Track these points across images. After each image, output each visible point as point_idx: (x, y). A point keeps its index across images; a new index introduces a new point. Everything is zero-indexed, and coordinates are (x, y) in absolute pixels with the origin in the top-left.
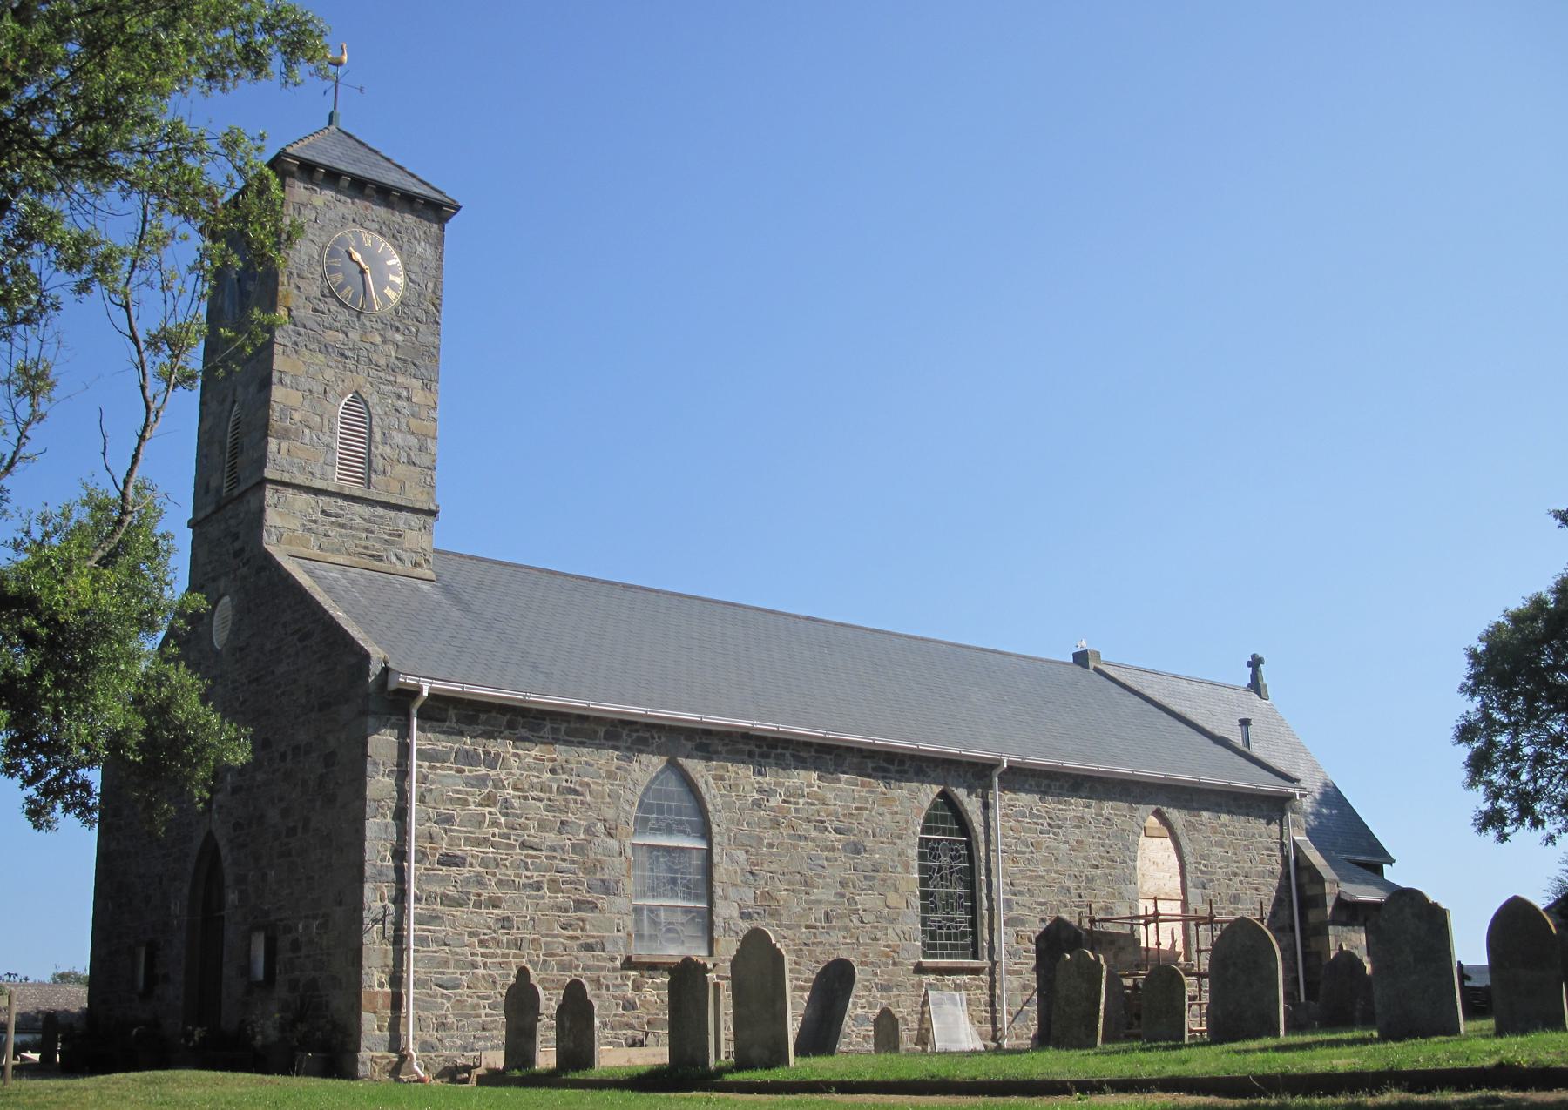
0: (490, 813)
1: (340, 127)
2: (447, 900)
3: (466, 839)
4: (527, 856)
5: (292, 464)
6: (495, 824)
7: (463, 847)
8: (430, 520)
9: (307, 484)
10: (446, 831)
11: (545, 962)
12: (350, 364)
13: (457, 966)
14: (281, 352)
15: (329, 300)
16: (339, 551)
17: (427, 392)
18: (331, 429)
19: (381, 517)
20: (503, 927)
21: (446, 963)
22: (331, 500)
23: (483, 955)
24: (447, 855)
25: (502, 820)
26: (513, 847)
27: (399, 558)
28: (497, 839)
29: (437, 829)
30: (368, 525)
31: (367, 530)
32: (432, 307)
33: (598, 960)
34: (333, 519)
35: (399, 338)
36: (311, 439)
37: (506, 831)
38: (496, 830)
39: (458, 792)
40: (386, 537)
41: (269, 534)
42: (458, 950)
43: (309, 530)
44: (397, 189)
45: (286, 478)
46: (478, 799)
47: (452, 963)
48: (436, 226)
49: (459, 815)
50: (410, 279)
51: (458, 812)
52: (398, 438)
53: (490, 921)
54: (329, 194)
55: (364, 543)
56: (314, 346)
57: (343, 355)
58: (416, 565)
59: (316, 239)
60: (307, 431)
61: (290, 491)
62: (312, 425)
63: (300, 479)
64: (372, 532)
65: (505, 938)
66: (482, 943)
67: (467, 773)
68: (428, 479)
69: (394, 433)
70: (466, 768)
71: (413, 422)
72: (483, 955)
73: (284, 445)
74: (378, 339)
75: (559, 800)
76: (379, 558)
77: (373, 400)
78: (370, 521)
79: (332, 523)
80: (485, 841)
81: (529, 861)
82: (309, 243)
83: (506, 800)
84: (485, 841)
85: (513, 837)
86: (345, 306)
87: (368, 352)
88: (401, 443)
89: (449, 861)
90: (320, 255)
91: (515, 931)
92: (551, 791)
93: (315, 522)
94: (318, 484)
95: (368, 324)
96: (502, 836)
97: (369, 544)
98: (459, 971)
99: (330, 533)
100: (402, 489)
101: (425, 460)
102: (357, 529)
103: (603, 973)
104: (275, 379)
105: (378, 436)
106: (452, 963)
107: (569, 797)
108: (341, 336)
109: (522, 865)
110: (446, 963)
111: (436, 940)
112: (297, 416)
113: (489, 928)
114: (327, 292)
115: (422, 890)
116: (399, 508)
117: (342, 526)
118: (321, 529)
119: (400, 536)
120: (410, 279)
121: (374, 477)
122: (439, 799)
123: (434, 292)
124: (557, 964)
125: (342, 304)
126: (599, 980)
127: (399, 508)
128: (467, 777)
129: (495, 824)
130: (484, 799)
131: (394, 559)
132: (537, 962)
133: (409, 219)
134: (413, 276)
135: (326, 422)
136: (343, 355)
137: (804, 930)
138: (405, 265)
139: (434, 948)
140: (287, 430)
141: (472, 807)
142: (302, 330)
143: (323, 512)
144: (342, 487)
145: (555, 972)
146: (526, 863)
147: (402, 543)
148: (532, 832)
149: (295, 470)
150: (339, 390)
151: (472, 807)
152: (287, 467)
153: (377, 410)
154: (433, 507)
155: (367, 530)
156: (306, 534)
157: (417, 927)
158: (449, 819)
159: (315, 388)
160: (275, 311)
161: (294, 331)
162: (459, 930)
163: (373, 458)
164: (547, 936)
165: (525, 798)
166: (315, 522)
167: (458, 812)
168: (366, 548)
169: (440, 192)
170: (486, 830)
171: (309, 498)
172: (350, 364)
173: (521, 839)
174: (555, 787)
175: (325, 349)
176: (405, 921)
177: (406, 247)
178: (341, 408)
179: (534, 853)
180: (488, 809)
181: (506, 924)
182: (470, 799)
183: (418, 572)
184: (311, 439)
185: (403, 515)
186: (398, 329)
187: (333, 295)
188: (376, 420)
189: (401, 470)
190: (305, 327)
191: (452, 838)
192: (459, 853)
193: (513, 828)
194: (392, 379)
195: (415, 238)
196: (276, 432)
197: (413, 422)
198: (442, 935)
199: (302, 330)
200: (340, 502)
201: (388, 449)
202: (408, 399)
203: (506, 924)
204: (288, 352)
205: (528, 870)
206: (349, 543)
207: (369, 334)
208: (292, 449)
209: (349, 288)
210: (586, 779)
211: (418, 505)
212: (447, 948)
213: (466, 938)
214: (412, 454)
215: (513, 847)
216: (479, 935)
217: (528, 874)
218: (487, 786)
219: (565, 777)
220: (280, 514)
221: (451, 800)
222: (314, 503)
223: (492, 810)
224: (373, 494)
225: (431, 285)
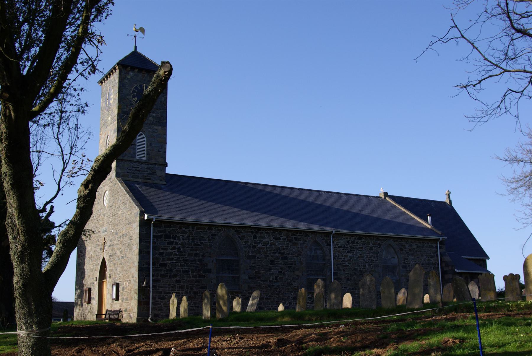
6: (175, 254)
11: (190, 292)
37: (178, 256)
38: (176, 256)
46: (171, 248)
76: (150, 179)
84: (172, 259)
106: (163, 293)
129: (175, 254)
145: (193, 295)
151: (169, 250)
156: (128, 174)
182: (168, 248)
213: (167, 286)
215: (180, 261)
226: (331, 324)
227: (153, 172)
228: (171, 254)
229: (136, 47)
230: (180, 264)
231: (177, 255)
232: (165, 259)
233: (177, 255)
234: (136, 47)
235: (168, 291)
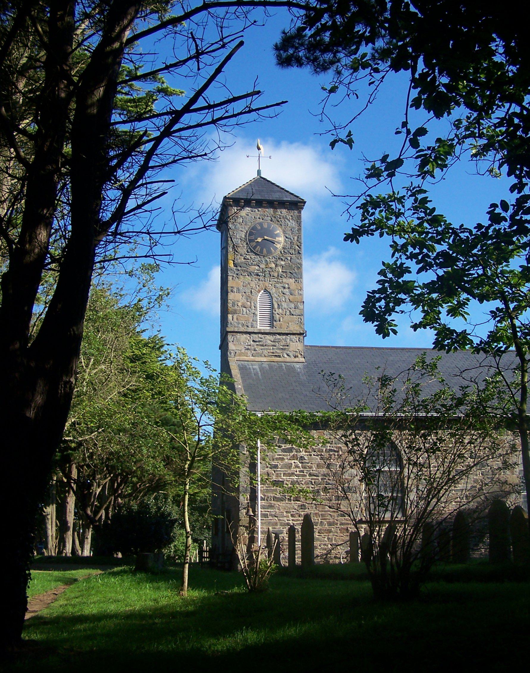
0: (294, 463)
1: (262, 176)
2: (275, 499)
3: (284, 474)
4: (312, 479)
5: (239, 323)
6: (297, 467)
7: (282, 477)
8: (301, 337)
9: (245, 331)
10: (274, 471)
11: (321, 522)
12: (261, 278)
13: (281, 525)
14: (231, 279)
15: (250, 254)
16: (261, 356)
17: (297, 283)
18: (255, 307)
19: (279, 339)
20: (302, 509)
21: (276, 524)
22: (256, 336)
23: (293, 520)
24: (275, 481)
25: (300, 465)
26: (306, 476)
27: (288, 355)
28: (298, 473)
29: (271, 471)
30: (273, 343)
31: (273, 346)
32: (297, 247)
33: (347, 520)
34: (257, 343)
35: (283, 263)
36: (246, 312)
37: (302, 469)
38: (298, 469)
39: (280, 455)
40: (282, 347)
41: (230, 353)
42: (281, 518)
43: (248, 349)
44: (276, 201)
45: (236, 330)
46: (289, 457)
47: (279, 524)
48: (296, 212)
49: (280, 464)
50: (286, 237)
51: (280, 463)
52: (284, 305)
53: (296, 507)
54: (248, 209)
55: (272, 351)
56: (246, 274)
57: (258, 275)
58: (296, 357)
59: (243, 230)
60: (244, 309)
61: (239, 334)
62: (246, 306)
63: (242, 329)
64: (275, 346)
65: (302, 513)
66: (292, 516)
67: (283, 447)
68: (300, 320)
69: (283, 303)
70: (283, 445)
71: (291, 297)
72: (293, 520)
73: (235, 316)
74: (273, 265)
75: (326, 455)
76: (279, 356)
77: (273, 291)
78: (274, 342)
79: (257, 345)
80: (293, 474)
81: (313, 481)
82: (240, 232)
83: (301, 457)
84: (293, 474)
85: (305, 472)
86: (258, 255)
87: (269, 272)
88: (286, 307)
89: (276, 483)
90: (245, 236)
91: (307, 510)
92: (322, 452)
93: (250, 345)
94: (250, 330)
95: (268, 260)
96: (300, 471)
97: (274, 351)
98: (282, 527)
99: (257, 349)
100: (288, 327)
101: (297, 312)
102: (269, 346)
103: (350, 526)
104: (229, 291)
105: (276, 306)
106: (279, 524)
107: (332, 453)
108: (257, 268)
109: (310, 483)
110: (276, 524)
111: (271, 515)
112: (240, 304)
113: (295, 509)
114: (249, 250)
115: (265, 496)
116: (287, 334)
117: (262, 345)
118: (252, 348)
119: (288, 346)
120: (286, 237)
121: (275, 323)
122: (271, 459)
123: (297, 241)
124: (327, 523)
125: (256, 254)
126: (347, 529)
127: (287, 334)
128: (283, 449)
129: (297, 467)
130: (291, 457)
131: (286, 356)
132: (318, 522)
133: (284, 211)
134: (287, 236)
135: (253, 304)
136: (258, 275)
137: (454, 503)
138: (284, 232)
139: (270, 518)
140: (235, 310)
141: (286, 461)
142: (239, 268)
143: (253, 341)
144: (260, 330)
145: (326, 526)
146: (312, 482)
147: (288, 349)
148: (314, 469)
149: (240, 326)
150: (257, 290)
151: (286, 461)
152: (236, 325)
153: (275, 295)
154: (302, 332)
155: (273, 346)
156: (246, 351)
157: (263, 510)
158: (276, 466)
159: (247, 291)
160: (277, 248)
161: (236, 269)
162: (282, 510)
163: (274, 315)
164: (322, 511)
165: (311, 455)
166: (250, 345)
167: (280, 463)
168: (273, 353)
169: (297, 197)
170: (293, 470)
171: (247, 336)
172: (261, 278)
173: (309, 472)
174: (325, 449)
175: (250, 274)
176: (256, 508)
177: (283, 224)
178: (259, 297)
179: (315, 478)
180: (294, 461)
181: (303, 507)
182: (285, 458)
183: (296, 360)
184: (246, 312)
185: (288, 337)
186: (282, 259)
187: (252, 251)
188: (274, 299)
189: (288, 317)
190: (241, 267)
191: (277, 474)
192: (281, 480)
193: (305, 468)
194: (281, 281)
195: (287, 219)
196: (231, 311)
197: (291, 297)
198: (273, 513)
199: (239, 268)
200: (260, 335)
201: (280, 310)
202: (289, 288)
203: (303, 507)
204: (234, 278)
205: (313, 485)
206: (265, 352)
207: (269, 264)
208: (238, 317)
209: (258, 247)
210: (340, 445)
211: (295, 332)
212: (276, 518)
213: (285, 513)
214: (291, 310)
215: (306, 476)
216: (290, 512)
217: (313, 486)
218: (292, 452)
219: (329, 445)
220: (234, 345)
221: (277, 459)
222: (249, 338)
223: (296, 461)
224: (274, 330)
225: (296, 238)
226: (254, 511)
227: (285, 346)
228: (289, 466)
229: (259, 172)
230: (304, 481)
231: (298, 467)
232: (281, 474)
233: (298, 467)
234: (259, 172)
235: (287, 521)
